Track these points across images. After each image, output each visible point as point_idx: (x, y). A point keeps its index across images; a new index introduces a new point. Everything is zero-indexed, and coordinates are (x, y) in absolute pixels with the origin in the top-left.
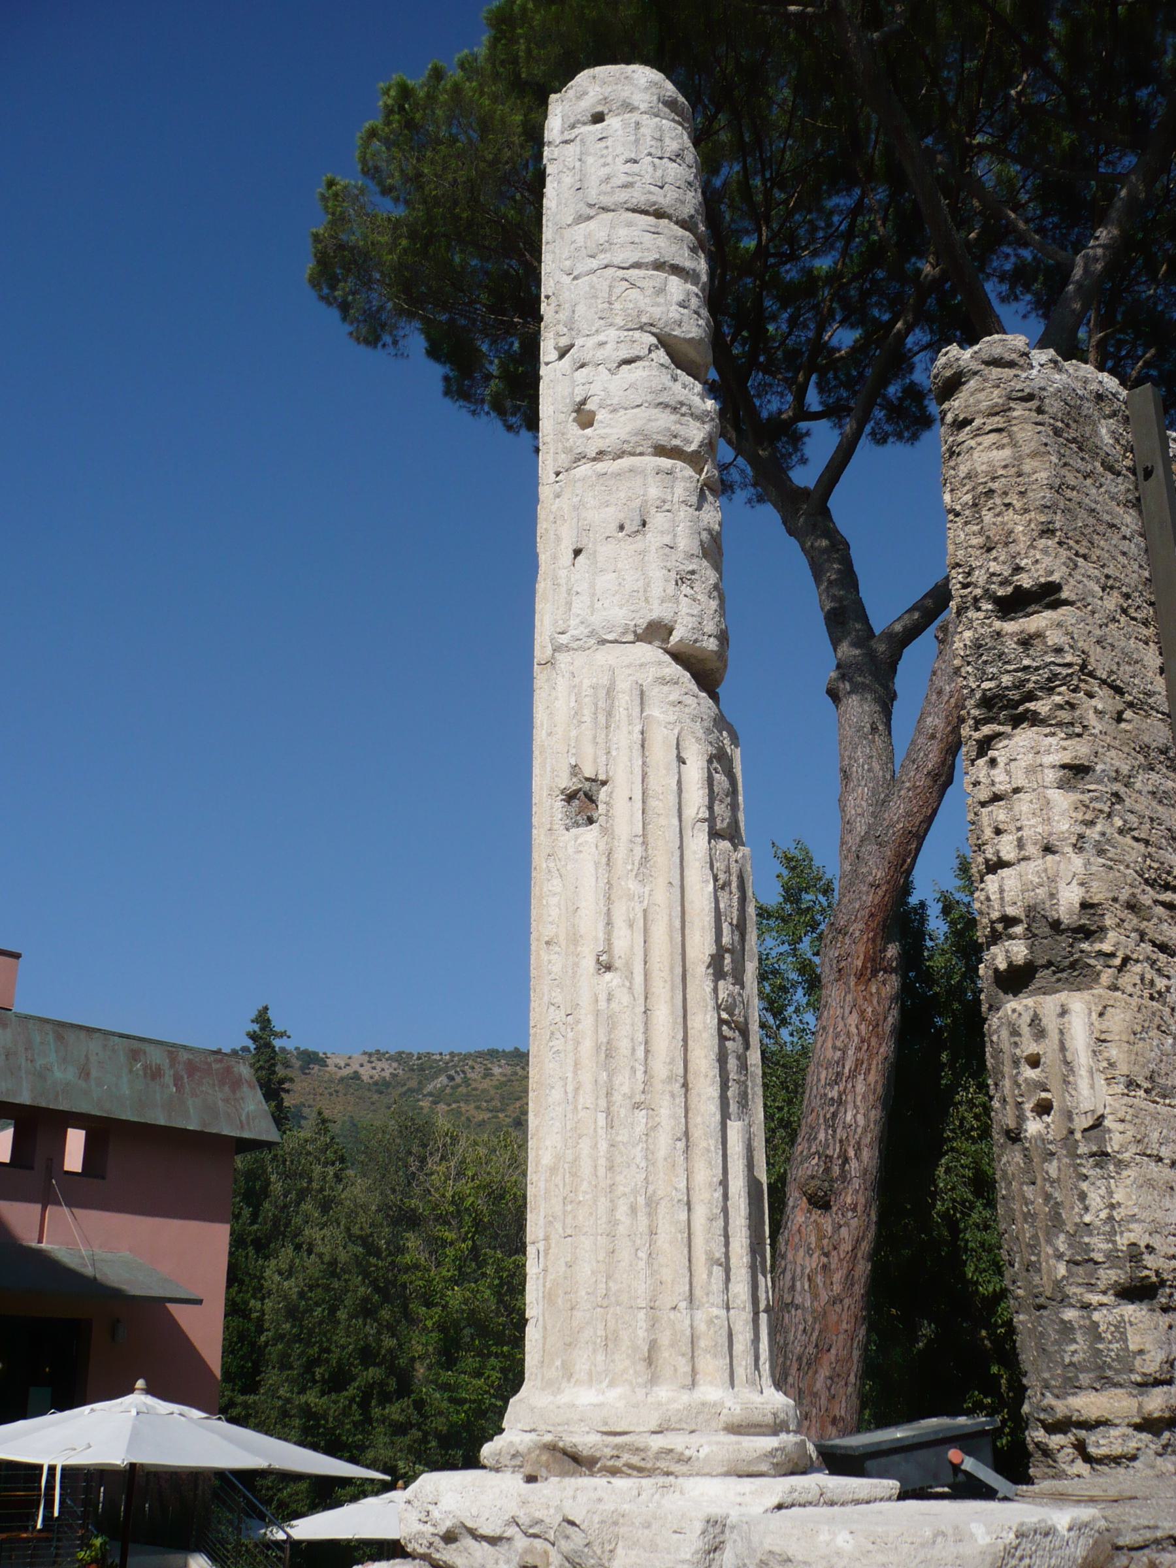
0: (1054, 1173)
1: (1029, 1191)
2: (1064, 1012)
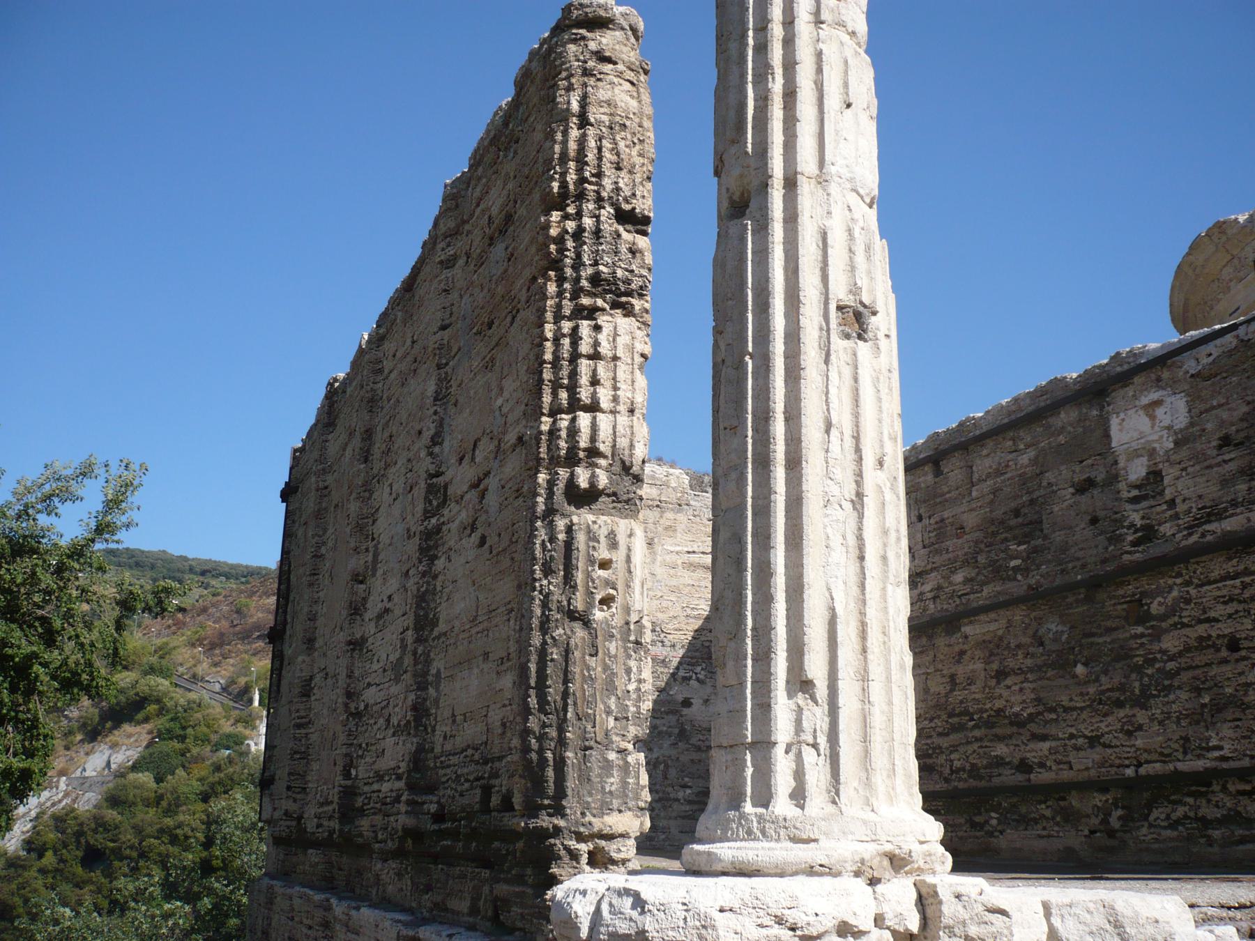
0: (613, 651)
1: (592, 662)
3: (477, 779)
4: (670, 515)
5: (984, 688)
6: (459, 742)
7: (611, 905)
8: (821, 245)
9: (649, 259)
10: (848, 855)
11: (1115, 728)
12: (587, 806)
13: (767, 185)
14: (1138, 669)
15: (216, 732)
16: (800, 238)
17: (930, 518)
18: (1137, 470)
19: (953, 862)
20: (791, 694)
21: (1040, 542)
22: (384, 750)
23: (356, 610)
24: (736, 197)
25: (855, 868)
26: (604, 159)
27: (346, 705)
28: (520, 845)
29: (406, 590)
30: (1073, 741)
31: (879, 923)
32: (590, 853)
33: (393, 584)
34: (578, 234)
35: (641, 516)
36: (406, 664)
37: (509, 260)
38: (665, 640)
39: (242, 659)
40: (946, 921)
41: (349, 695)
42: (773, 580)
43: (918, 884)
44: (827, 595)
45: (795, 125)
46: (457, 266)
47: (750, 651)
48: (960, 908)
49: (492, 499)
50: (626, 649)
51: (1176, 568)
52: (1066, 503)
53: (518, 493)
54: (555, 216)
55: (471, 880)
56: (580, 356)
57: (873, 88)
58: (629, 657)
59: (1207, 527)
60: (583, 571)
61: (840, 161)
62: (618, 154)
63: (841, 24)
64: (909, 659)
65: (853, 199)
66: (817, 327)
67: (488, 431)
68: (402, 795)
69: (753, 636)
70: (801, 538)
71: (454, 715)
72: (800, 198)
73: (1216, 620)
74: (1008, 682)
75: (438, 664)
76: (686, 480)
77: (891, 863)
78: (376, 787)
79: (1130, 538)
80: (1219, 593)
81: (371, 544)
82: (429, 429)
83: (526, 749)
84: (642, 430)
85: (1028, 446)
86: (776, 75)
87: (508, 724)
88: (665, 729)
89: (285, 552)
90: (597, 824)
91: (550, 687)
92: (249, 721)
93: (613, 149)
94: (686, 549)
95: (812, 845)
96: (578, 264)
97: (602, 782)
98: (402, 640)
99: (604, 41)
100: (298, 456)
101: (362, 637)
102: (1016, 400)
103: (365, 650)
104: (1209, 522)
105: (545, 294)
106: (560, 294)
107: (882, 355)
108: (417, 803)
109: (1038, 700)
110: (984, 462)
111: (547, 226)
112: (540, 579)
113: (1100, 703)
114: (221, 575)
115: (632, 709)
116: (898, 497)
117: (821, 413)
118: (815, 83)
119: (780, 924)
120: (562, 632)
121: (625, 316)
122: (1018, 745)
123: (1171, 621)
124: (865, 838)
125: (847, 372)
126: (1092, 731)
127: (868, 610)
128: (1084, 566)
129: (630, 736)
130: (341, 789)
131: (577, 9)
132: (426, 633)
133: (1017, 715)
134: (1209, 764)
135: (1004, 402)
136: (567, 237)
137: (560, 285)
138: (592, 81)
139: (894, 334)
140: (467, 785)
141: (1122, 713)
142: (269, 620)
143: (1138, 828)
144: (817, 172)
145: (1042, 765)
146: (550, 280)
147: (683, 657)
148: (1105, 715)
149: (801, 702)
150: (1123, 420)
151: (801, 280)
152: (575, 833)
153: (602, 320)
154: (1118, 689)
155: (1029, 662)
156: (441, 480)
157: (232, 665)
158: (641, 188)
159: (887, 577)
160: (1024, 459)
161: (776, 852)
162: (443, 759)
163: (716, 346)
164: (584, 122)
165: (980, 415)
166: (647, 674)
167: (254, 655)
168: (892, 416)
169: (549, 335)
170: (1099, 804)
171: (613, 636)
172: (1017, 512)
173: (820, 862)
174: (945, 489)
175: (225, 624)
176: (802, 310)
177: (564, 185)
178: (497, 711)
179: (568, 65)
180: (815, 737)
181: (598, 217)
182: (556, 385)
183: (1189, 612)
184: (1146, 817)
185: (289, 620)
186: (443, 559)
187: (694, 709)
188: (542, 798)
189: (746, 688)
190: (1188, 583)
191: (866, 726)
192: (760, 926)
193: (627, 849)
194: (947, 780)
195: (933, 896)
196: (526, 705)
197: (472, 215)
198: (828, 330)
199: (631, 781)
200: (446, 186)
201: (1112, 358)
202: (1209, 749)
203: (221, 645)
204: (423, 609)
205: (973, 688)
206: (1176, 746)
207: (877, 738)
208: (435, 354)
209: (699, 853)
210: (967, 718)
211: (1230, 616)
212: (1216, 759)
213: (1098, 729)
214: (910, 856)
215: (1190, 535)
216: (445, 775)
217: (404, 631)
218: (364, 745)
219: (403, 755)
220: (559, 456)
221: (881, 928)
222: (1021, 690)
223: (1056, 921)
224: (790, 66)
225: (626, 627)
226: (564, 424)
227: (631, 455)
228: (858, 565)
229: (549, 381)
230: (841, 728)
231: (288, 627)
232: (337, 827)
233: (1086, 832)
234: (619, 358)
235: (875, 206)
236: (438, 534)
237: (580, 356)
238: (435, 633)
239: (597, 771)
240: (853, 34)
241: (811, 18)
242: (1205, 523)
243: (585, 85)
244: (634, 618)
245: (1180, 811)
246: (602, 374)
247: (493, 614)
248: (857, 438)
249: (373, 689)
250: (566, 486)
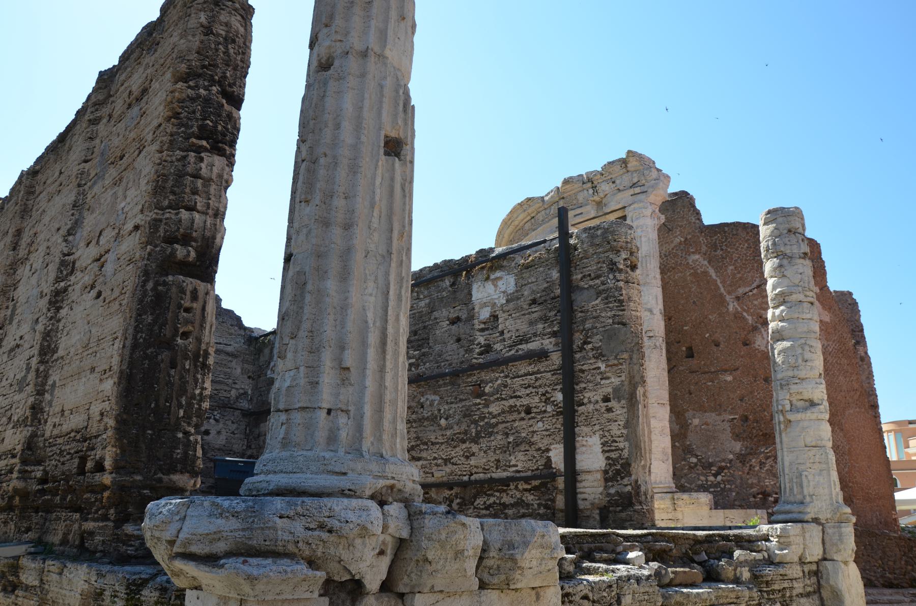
3: (76, 452)
6: (65, 428)
14: (475, 422)
18: (485, 314)
21: (427, 350)
33: (25, 328)
36: (29, 379)
37: (142, 116)
46: (101, 123)
49: (109, 268)
51: (501, 368)
55: (64, 521)
59: (520, 347)
62: (229, 56)
71: (63, 411)
73: (520, 397)
75: (55, 377)
79: (477, 350)
80: (523, 383)
81: (11, 304)
85: (425, 297)
87: (105, 413)
98: (28, 364)
104: (521, 344)
108: (27, 471)
109: (418, 438)
123: (495, 397)
128: (450, 365)
134: (509, 474)
140: (68, 457)
141: (464, 446)
143: (468, 509)
148: (455, 447)
154: (464, 433)
156: (71, 258)
160: (422, 304)
162: (51, 441)
178: (97, 405)
183: (505, 393)
184: (473, 504)
187: (211, 436)
190: (506, 377)
202: (510, 467)
204: (47, 341)
206: (492, 464)
208: (77, 178)
211: (528, 395)
212: (513, 472)
215: (510, 350)
236: (64, 292)
242: (519, 344)
245: (492, 500)
247: (102, 341)
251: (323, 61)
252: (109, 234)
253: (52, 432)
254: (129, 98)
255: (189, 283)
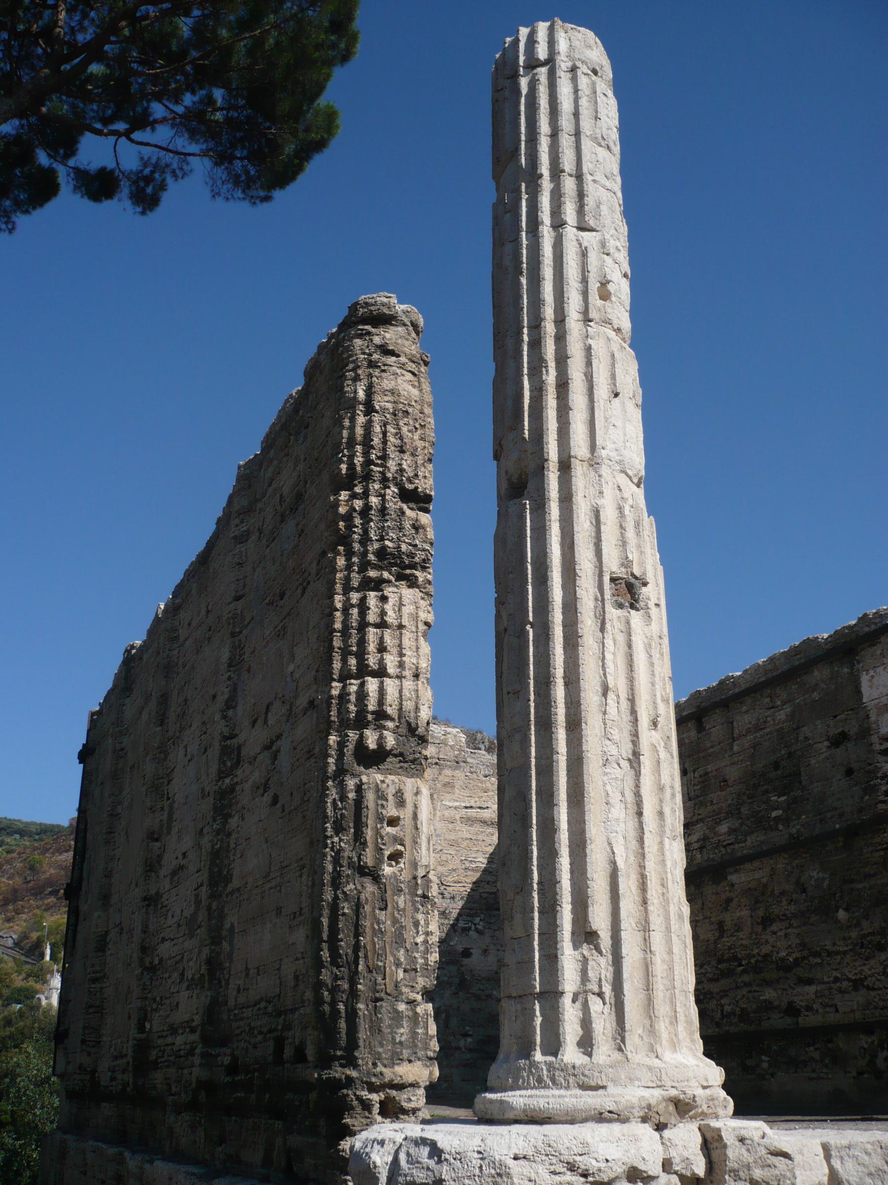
0: (401, 905)
1: (382, 915)
2: (417, 793)
3: (271, 1031)
4: (448, 772)
5: (751, 934)
7: (408, 1154)
8: (594, 522)
9: (431, 534)
10: (635, 1101)
11: (877, 971)
12: (378, 1057)
13: (544, 467)
15: (8, 986)
16: (575, 516)
17: (694, 771)
19: (735, 1106)
20: (576, 946)
22: (178, 1004)
23: (151, 867)
24: (514, 479)
25: (642, 1114)
26: (389, 443)
27: (141, 960)
28: (313, 1096)
29: (200, 847)
30: (838, 984)
31: (667, 1167)
32: (381, 1102)
33: (187, 842)
34: (365, 512)
35: (426, 775)
36: (200, 919)
37: (300, 535)
38: (445, 892)
39: (35, 915)
40: (731, 1164)
41: (144, 949)
42: (556, 836)
43: (702, 1129)
44: (608, 849)
45: (568, 413)
46: (250, 541)
47: (536, 904)
48: (744, 1151)
49: (284, 759)
50: (414, 903)
52: (823, 756)
53: (310, 754)
54: (344, 495)
56: (369, 624)
57: (638, 379)
58: (417, 910)
60: (372, 828)
61: (610, 446)
62: (401, 438)
63: (608, 322)
64: (686, 910)
65: (622, 479)
66: (592, 598)
67: (280, 696)
68: (195, 1048)
69: (539, 890)
70: (583, 796)
71: (247, 969)
72: (574, 479)
74: (774, 927)
75: (232, 919)
76: (463, 738)
77: (676, 1108)
78: (170, 1040)
81: (167, 803)
82: (223, 693)
83: (319, 1001)
84: (427, 694)
85: (784, 703)
86: (550, 369)
87: (301, 977)
88: (446, 979)
89: (81, 810)
90: (388, 1073)
91: (341, 940)
92: (41, 976)
93: (397, 434)
94: (464, 805)
95: (601, 1092)
96: (365, 539)
97: (393, 1033)
98: (197, 896)
99: (388, 336)
100: (95, 720)
101: (157, 893)
102: (771, 659)
103: (160, 906)
105: (335, 568)
106: (349, 567)
107: (653, 623)
110: (744, 719)
111: (336, 504)
112: (331, 837)
113: (862, 947)
114: (16, 833)
115: (421, 961)
116: (672, 755)
117: (598, 678)
118: (585, 375)
119: (572, 1171)
120: (354, 887)
121: (409, 587)
122: (785, 990)
124: (651, 1084)
125: (621, 638)
126: (856, 974)
127: (647, 863)
129: (419, 987)
130: (135, 1042)
131: (362, 307)
132: (220, 889)
133: (783, 960)
135: (761, 661)
136: (355, 514)
137: (348, 559)
138: (377, 372)
139: (663, 603)
140: (260, 1038)
142: (63, 877)
144: (589, 455)
145: (809, 1008)
146: (339, 554)
147: (463, 908)
148: (868, 959)
149: (585, 952)
150: (873, 677)
151: (577, 555)
152: (367, 1083)
153: (388, 591)
155: (792, 908)
157: (25, 921)
158: (423, 469)
159: (664, 832)
160: (781, 715)
161: (567, 1100)
162: (236, 1012)
163: (498, 616)
164: (370, 409)
165: (739, 674)
166: (433, 927)
167: (46, 910)
168: (664, 680)
169: (339, 605)
170: (866, 1046)
171: (401, 891)
172: (776, 765)
173: (608, 1108)
174: (708, 744)
175: (18, 880)
176: (578, 583)
177: (351, 466)
179: (354, 358)
180: (600, 986)
181: (383, 496)
182: (345, 653)
185: (85, 878)
186: (236, 818)
188: (335, 1050)
189: (534, 939)
191: (648, 975)
192: (554, 1173)
193: (418, 1098)
194: (718, 1025)
195: (718, 1140)
196: (319, 958)
197: (264, 495)
198: (603, 601)
199: (420, 1031)
200: (239, 467)
201: (860, 619)
203: (15, 901)
205: (741, 934)
207: (660, 986)
208: (229, 624)
209: (491, 1101)
210: (736, 964)
213: (861, 972)
214: (694, 1101)
216: (238, 1028)
217: (198, 887)
218: (158, 999)
219: (197, 1009)
220: (349, 719)
221: (669, 1173)
222: (786, 935)
223: (836, 1164)
224: (562, 359)
225: (413, 881)
226: (353, 689)
227: (417, 717)
228: (636, 820)
229: (339, 648)
230: (625, 977)
231: (84, 883)
232: (131, 1080)
233: (854, 1074)
234: (405, 626)
235: (642, 486)
237: (369, 624)
238: (229, 889)
239: (387, 1022)
240: (618, 330)
241: (580, 317)
243: (370, 376)
244: (421, 872)
246: (389, 641)
248: (632, 700)
249: (167, 944)
250: (356, 747)
251: (514, 479)
252: (278, 711)
253: (236, 1000)
254: (281, 506)
255: (390, 783)
